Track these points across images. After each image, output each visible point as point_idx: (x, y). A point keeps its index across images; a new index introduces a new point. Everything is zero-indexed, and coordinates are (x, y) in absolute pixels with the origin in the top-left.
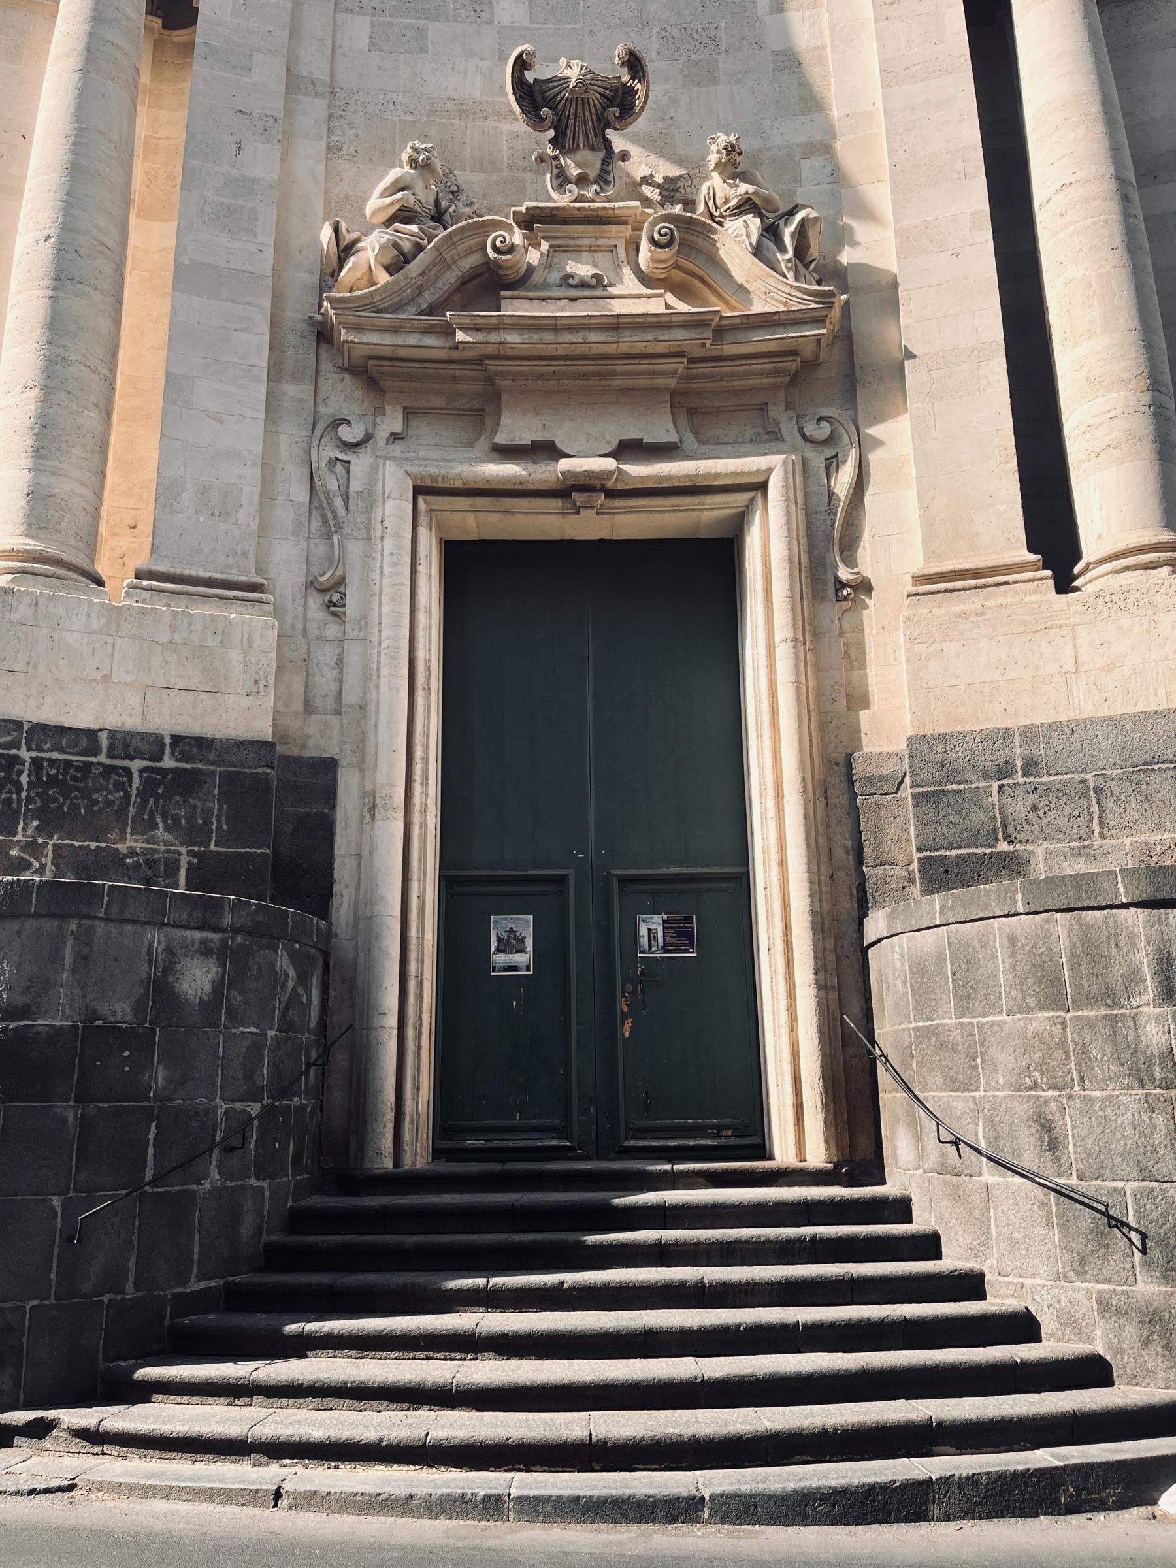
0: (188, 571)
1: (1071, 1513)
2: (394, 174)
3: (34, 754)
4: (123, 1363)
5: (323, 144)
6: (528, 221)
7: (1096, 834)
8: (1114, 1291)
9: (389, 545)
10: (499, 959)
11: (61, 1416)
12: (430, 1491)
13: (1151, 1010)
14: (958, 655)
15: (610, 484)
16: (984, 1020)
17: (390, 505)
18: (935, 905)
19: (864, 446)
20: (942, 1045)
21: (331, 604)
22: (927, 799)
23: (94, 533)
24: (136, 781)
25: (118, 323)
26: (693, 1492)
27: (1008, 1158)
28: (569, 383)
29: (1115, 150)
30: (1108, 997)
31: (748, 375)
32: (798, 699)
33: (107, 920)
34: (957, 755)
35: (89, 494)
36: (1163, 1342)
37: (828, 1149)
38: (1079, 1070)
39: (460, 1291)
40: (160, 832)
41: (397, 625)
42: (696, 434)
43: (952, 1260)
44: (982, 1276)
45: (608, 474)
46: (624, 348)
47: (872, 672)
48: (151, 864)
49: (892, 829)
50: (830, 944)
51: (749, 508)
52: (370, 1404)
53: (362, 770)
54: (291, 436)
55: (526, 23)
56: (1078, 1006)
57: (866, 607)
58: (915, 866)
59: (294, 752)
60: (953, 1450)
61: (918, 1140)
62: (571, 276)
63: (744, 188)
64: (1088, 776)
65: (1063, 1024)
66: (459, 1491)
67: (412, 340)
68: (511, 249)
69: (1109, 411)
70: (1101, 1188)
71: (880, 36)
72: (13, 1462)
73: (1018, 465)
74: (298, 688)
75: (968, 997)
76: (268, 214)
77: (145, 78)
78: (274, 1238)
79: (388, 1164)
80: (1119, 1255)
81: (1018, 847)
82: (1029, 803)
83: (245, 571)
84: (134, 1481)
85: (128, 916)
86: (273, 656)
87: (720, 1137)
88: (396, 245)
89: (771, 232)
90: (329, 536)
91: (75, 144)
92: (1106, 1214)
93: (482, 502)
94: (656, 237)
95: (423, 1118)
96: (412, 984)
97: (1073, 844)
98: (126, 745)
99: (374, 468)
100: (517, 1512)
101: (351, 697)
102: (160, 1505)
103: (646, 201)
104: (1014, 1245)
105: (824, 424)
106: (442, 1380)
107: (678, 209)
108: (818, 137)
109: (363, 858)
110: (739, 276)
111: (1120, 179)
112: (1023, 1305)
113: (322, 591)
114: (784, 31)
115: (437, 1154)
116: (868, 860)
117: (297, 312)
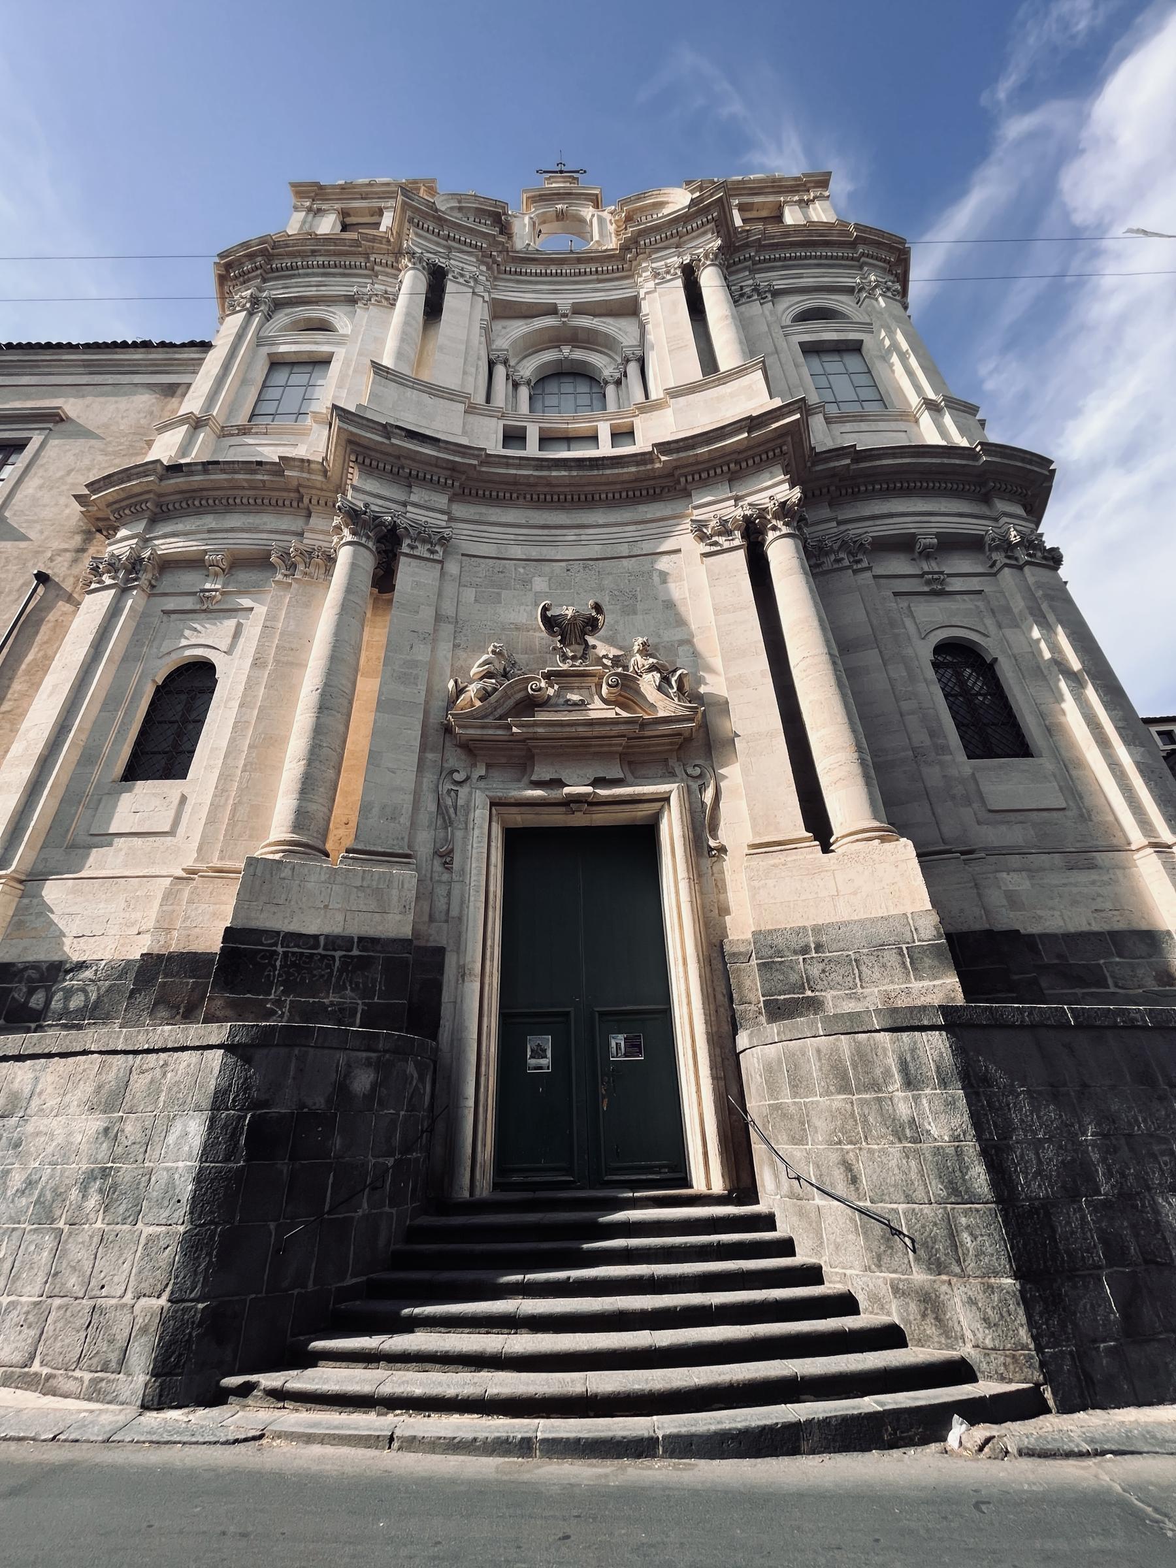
0: (373, 849)
1: (892, 1448)
2: (485, 657)
3: (285, 949)
4: (302, 1338)
5: (451, 645)
6: (548, 676)
7: (859, 985)
8: (900, 1279)
9: (477, 832)
10: (532, 1062)
11: (261, 1380)
12: (486, 1435)
13: (900, 1094)
14: (775, 886)
15: (590, 799)
16: (807, 1100)
17: (478, 812)
18: (774, 1029)
19: (718, 779)
20: (784, 1115)
21: (446, 863)
22: (764, 967)
23: (327, 829)
24: (337, 963)
25: (347, 727)
26: (652, 1434)
27: (828, 1189)
28: (568, 750)
29: (827, 642)
30: (875, 1086)
31: (658, 745)
32: (693, 910)
33: (316, 1047)
34: (780, 942)
35: (326, 810)
36: (934, 1316)
37: (724, 1182)
38: (864, 1132)
39: (508, 1284)
40: (348, 992)
41: (479, 874)
42: (633, 774)
43: (802, 1257)
44: (820, 1268)
45: (589, 794)
46: (595, 734)
47: (730, 894)
48: (342, 1010)
49: (748, 983)
50: (718, 1051)
51: (661, 810)
52: (452, 1367)
53: (458, 953)
54: (429, 778)
55: (547, 590)
56: (859, 1092)
57: (725, 860)
58: (762, 1004)
59: (422, 943)
60: (812, 1398)
61: (776, 1176)
62: (569, 700)
63: (651, 660)
64: (850, 953)
65: (852, 1103)
66: (505, 1435)
67: (491, 732)
68: (540, 689)
70: (884, 1208)
71: (711, 593)
72: (226, 1417)
74: (426, 908)
75: (797, 1086)
76: (424, 675)
77: (369, 615)
78: (398, 1246)
79: (466, 1194)
80: (900, 1254)
81: (817, 994)
82: (820, 968)
83: (401, 848)
84: (301, 1430)
85: (326, 1045)
86: (414, 892)
87: (660, 1173)
88: (484, 689)
89: (666, 679)
90: (446, 828)
91: (334, 646)
92: (889, 1226)
93: (523, 809)
95: (488, 1162)
96: (483, 1079)
97: (847, 992)
98: (333, 943)
99: (470, 793)
100: (541, 1451)
101: (454, 912)
102: (316, 1450)
103: (605, 666)
104: (837, 1247)
105: (697, 768)
106: (496, 1350)
107: (620, 670)
108: (686, 637)
109: (458, 1004)
110: (651, 699)
111: (831, 655)
112: (847, 1288)
113: (441, 856)
114: (667, 591)
115: (496, 1186)
116: (736, 1001)
117: (435, 719)
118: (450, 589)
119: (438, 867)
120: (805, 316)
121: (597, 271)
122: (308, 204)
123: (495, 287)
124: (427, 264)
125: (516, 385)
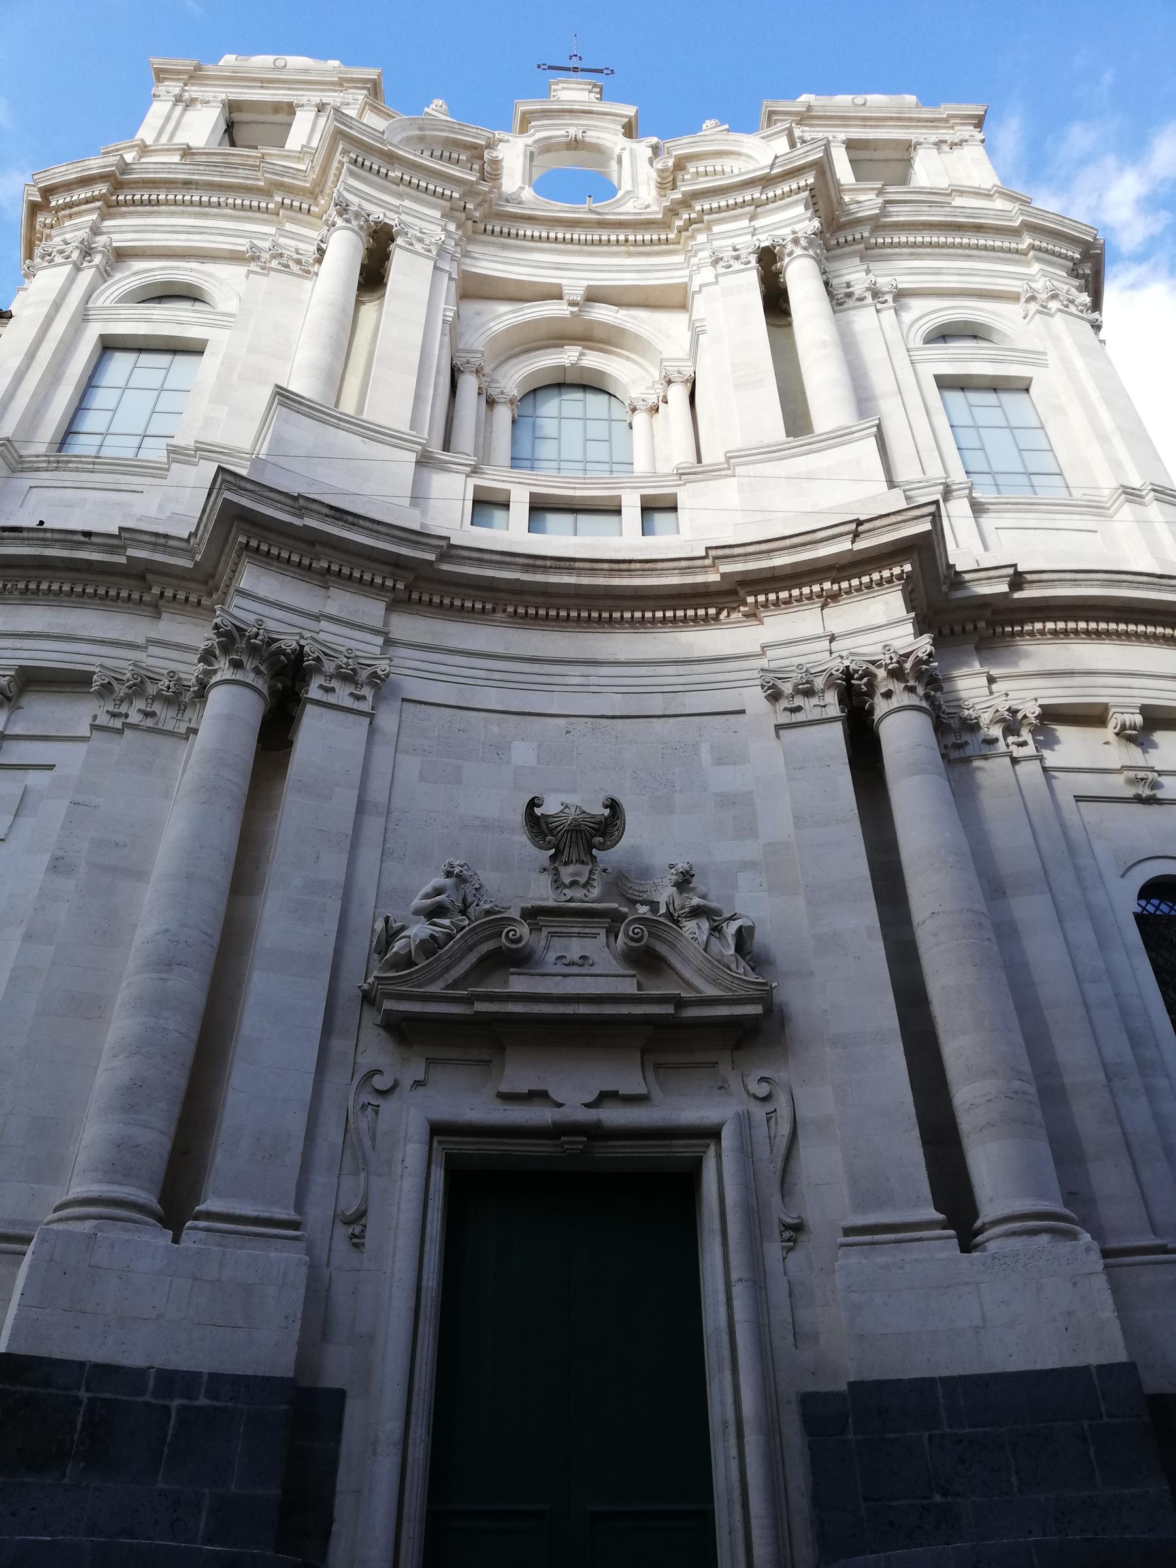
69: (985, 1095)
73: (920, 1133)
94: (631, 933)
118: (382, 755)
119: (341, 1245)
120: (943, 335)
121: (627, 241)
122: (177, 91)
123: (467, 254)
124: (367, 221)
125: (491, 403)
